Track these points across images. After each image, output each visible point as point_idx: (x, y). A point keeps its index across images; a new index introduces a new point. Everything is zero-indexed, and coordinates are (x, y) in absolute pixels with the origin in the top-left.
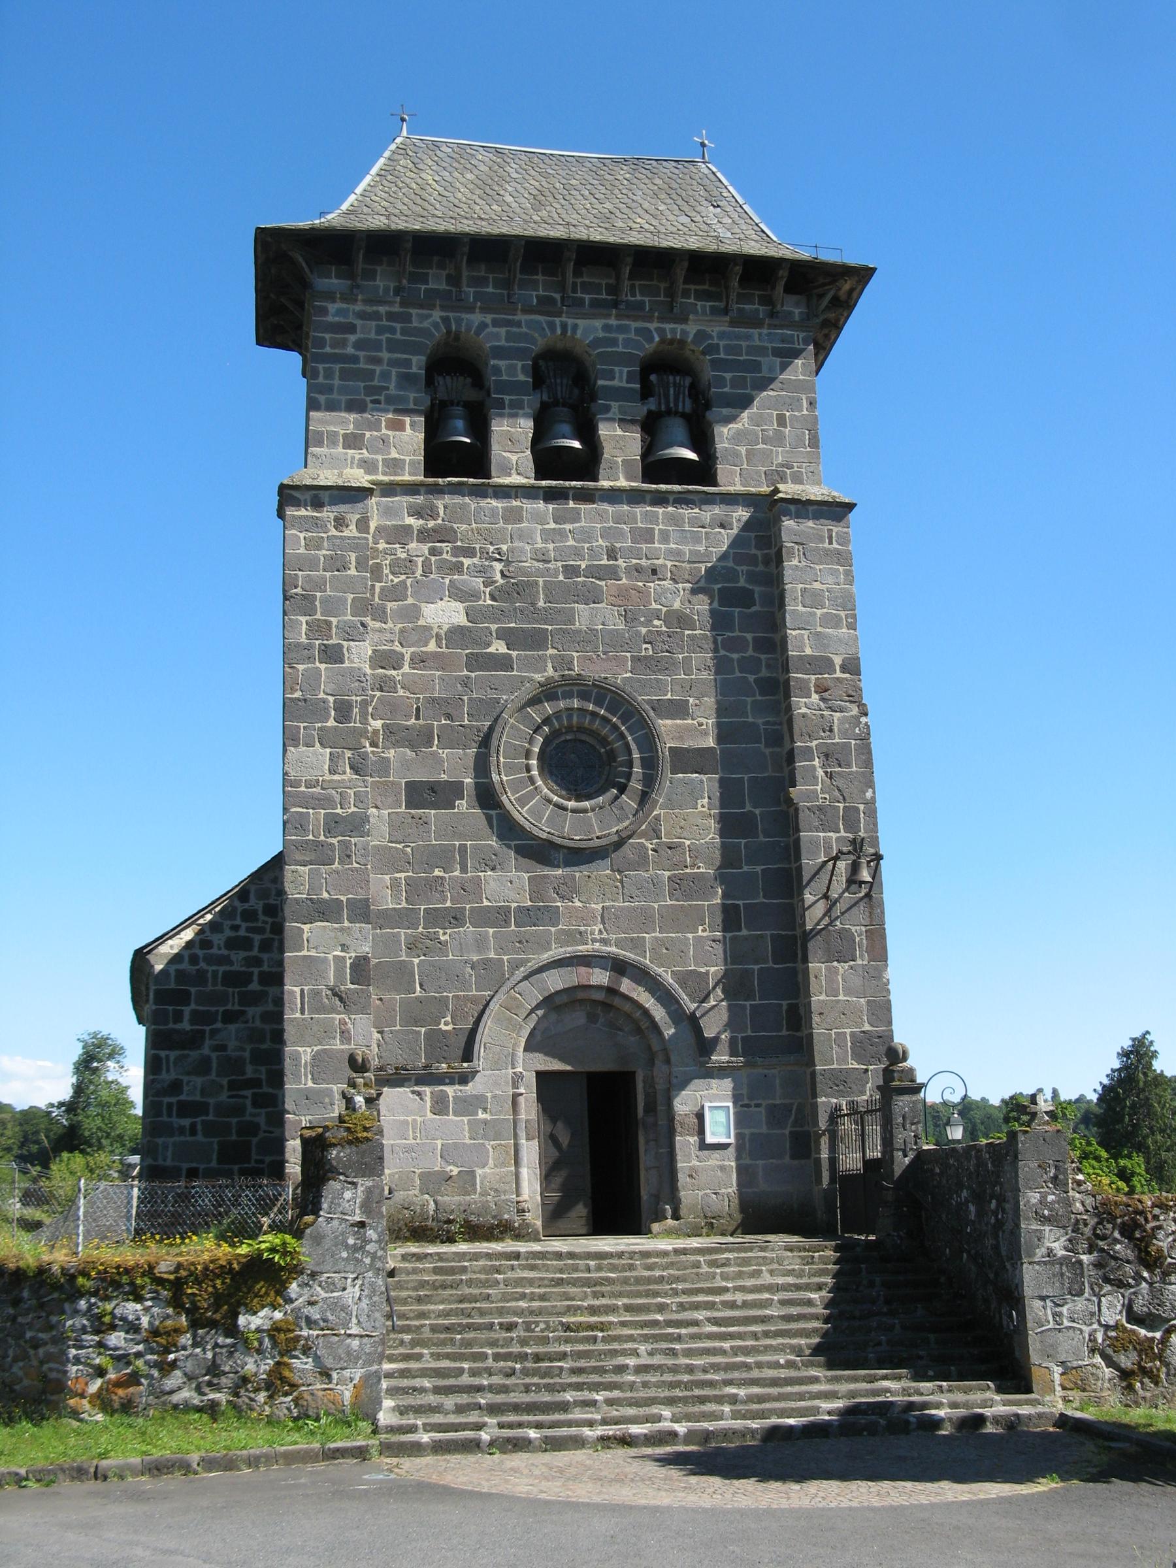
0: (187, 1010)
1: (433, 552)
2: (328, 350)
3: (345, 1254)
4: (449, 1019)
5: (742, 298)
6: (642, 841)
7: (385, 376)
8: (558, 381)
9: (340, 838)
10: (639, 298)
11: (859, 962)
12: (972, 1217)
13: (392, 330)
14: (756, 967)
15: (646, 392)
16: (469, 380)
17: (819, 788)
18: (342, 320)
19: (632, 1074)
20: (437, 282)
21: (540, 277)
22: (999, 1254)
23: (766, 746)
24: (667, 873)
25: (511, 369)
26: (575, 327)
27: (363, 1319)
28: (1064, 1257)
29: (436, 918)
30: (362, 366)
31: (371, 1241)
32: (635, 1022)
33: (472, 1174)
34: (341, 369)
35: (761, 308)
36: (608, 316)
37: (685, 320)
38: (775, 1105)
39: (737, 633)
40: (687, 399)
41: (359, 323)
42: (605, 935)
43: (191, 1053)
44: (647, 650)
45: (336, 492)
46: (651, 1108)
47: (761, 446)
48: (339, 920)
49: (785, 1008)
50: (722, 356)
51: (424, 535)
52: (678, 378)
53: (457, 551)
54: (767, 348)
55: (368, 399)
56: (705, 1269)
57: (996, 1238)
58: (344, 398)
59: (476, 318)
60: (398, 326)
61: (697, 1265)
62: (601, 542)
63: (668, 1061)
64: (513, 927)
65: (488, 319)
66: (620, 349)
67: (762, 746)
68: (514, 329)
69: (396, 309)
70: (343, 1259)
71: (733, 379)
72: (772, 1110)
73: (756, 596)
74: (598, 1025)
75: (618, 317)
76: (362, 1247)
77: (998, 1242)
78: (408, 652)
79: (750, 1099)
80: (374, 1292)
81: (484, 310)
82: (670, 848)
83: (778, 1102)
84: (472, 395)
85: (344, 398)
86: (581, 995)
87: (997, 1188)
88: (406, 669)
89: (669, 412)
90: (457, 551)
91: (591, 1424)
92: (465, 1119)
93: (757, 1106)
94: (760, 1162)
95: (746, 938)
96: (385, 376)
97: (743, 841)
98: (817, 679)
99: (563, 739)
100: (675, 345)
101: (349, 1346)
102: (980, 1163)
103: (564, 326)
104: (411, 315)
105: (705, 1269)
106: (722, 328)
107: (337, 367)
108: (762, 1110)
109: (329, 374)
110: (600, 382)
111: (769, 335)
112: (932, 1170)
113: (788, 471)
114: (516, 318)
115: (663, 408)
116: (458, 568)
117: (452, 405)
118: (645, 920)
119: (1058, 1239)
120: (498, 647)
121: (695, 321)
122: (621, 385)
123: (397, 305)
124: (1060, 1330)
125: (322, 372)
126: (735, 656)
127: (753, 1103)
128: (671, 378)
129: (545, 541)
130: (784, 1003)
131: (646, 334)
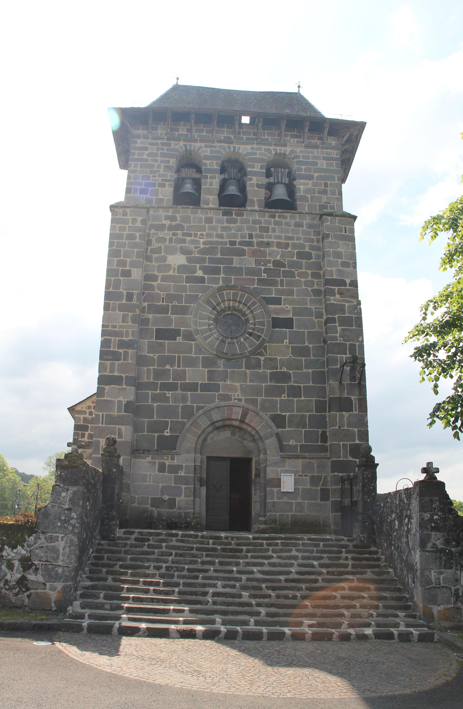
0: (87, 433)
1: (173, 234)
2: (136, 157)
3: (59, 524)
4: (168, 430)
5: (309, 138)
6: (259, 356)
7: (159, 167)
8: (232, 170)
9: (125, 350)
10: (266, 137)
11: (354, 412)
12: (397, 527)
13: (163, 149)
14: (308, 414)
15: (268, 174)
16: (195, 170)
17: (338, 335)
18: (143, 146)
19: (251, 459)
20: (182, 130)
21: (225, 129)
22: (408, 546)
23: (316, 318)
24: (269, 371)
25: (211, 164)
26: (239, 148)
27: (66, 558)
28: (442, 548)
29: (165, 387)
30: (149, 163)
31: (73, 518)
32: (253, 436)
33: (174, 500)
34: (141, 164)
35: (318, 141)
36: (253, 144)
37: (285, 145)
38: (314, 476)
39: (304, 270)
40: (286, 178)
41: (149, 146)
42: (240, 397)
43: (87, 450)
44: (264, 276)
45: (133, 209)
46: (258, 475)
47: (317, 195)
48: (120, 384)
49: (320, 433)
50: (301, 159)
51: (171, 228)
52: (283, 170)
53: (184, 234)
54: (321, 157)
55: (151, 175)
56: (265, 547)
57: (407, 537)
58: (141, 175)
59: (198, 145)
60: (165, 148)
61: (262, 545)
62: (246, 231)
63: (266, 453)
64: (199, 392)
65: (203, 145)
66: (258, 156)
67: (314, 318)
68: (213, 149)
69: (165, 141)
70: (58, 526)
71: (305, 169)
72: (312, 478)
73: (313, 255)
74: (236, 437)
75: (257, 144)
76: (68, 521)
77: (408, 540)
78: (160, 275)
79: (303, 472)
80: (72, 545)
81: (201, 141)
82: (270, 360)
83: (315, 474)
84: (196, 176)
85: (141, 175)
86: (228, 423)
87: (408, 512)
88: (159, 281)
89: (278, 183)
90: (184, 234)
91: (176, 622)
92: (173, 475)
93: (305, 476)
94: (306, 502)
95: (303, 401)
96: (159, 167)
97: (304, 358)
98: (338, 289)
99: (226, 313)
100: (282, 157)
101: (57, 571)
102: (401, 500)
103: (234, 148)
104: (171, 144)
105: (265, 547)
106: (302, 149)
107: (139, 163)
108: (308, 478)
109: (136, 166)
110: (249, 169)
111: (321, 152)
112: (380, 505)
113: (329, 205)
114: (215, 145)
115: (276, 181)
116: (184, 241)
117: (187, 179)
118: (258, 392)
119: (439, 539)
120: (200, 273)
121: (289, 146)
122: (257, 170)
123: (166, 140)
124: (439, 588)
125: (133, 165)
126: (303, 280)
127: (304, 475)
128: (280, 170)
129: (222, 231)
130: (320, 430)
131: (269, 151)
